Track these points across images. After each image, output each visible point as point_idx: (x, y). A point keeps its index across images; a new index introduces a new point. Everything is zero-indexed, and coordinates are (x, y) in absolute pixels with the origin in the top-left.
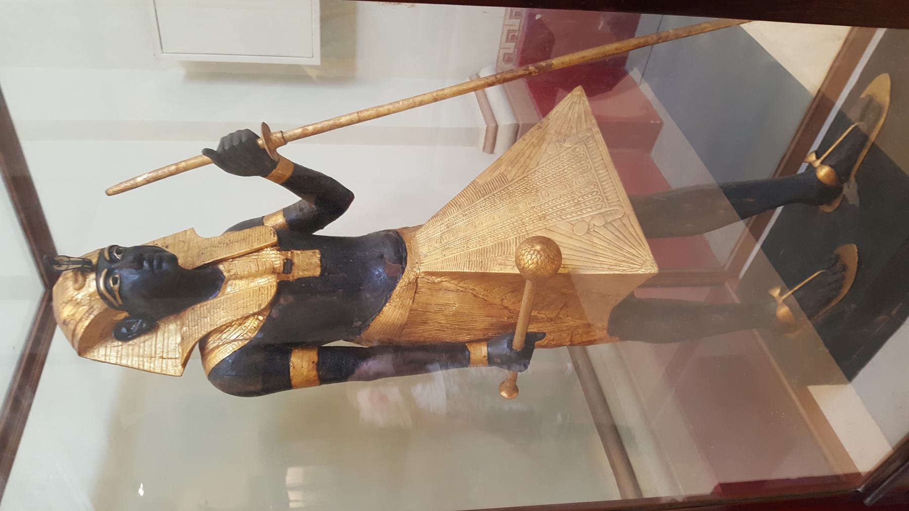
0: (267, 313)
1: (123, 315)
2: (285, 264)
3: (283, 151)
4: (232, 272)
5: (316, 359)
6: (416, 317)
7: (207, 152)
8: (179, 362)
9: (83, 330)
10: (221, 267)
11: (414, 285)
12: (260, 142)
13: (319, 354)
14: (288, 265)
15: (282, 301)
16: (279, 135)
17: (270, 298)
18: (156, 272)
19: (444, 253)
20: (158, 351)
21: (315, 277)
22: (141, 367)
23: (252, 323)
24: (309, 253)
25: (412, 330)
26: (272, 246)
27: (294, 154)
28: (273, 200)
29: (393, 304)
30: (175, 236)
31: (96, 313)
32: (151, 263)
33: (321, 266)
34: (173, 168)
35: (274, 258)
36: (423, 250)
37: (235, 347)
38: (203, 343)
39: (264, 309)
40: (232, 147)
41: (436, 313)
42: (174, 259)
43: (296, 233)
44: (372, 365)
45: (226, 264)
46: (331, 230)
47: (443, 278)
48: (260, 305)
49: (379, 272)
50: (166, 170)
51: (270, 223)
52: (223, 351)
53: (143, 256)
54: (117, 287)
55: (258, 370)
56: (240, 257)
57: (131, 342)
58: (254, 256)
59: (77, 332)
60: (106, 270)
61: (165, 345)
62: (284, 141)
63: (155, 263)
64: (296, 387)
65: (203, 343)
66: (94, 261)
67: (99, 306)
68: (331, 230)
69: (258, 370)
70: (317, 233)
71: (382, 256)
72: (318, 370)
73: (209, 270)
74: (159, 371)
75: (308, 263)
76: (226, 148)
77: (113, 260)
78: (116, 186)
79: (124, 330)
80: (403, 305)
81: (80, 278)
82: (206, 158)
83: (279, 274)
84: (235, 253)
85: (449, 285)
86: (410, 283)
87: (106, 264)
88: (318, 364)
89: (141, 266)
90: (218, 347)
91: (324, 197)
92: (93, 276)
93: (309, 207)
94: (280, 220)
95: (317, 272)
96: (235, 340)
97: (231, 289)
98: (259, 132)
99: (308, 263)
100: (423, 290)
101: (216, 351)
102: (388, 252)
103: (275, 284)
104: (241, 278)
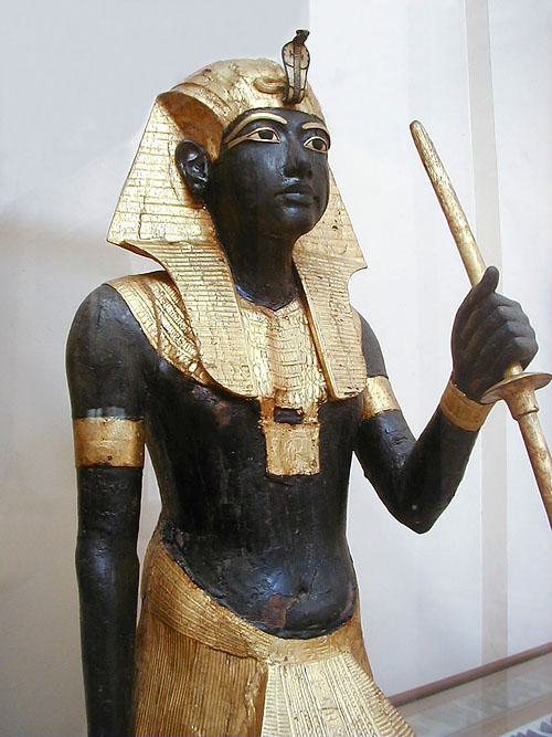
0: (201, 378)
1: (215, 155)
2: (294, 410)
3: (500, 412)
4: (283, 323)
5: (115, 463)
6: (182, 646)
7: (492, 277)
8: (132, 238)
9: (192, 95)
10: (295, 305)
11: (240, 652)
12: (515, 370)
13: (125, 467)
14: (291, 417)
15: (222, 405)
16: (531, 407)
17: (225, 384)
18: (280, 197)
19: (302, 717)
20: (155, 209)
21: (265, 465)
22: (130, 182)
23: (185, 354)
24: (314, 454)
25: (162, 641)
26: (329, 390)
27: (497, 429)
28: (414, 390)
29: (208, 610)
30: (354, 241)
31: (217, 111)
32: (292, 189)
33: (286, 477)
34: (461, 223)
35: (305, 394)
36: (315, 671)
37: (149, 328)
38: (164, 277)
39: (207, 374)
40: (503, 320)
41: (189, 693)
42: (304, 227)
43: (351, 429)
44: (102, 564)
45: (300, 313)
46: (361, 490)
47: (252, 711)
48: (214, 367)
49: (273, 584)
50: (456, 210)
51: (374, 386)
52: (137, 303)
53: (310, 184)
54: (256, 137)
55: (108, 365)
56: (311, 335)
57: (174, 168)
58: (311, 358)
59: (191, 88)
60: (285, 122)
61: (163, 219)
62: (519, 415)
63: (296, 196)
64: (75, 425)
65: (164, 277)
66: (302, 107)
67: (225, 114)
68: (361, 490)
69: (108, 365)
70: (355, 461)
71: (303, 589)
72: (96, 466)
73: (289, 286)
74: (121, 208)
75: (293, 452)
76: (502, 309)
77: (301, 133)
78: (426, 136)
79: (193, 156)
80: (204, 629)
81: (273, 86)
82: (480, 276)
83: (275, 400)
84: (319, 334)
85: (240, 721)
86: (247, 644)
87: (295, 124)
88: (107, 466)
89: (289, 174)
90: (152, 298)
91: (421, 480)
92: (276, 103)
93: (402, 452)
94: (379, 403)
95: (275, 469)
96: (159, 324)
97: (253, 322)
98: (535, 367)
99: (293, 452)
100: (232, 669)
101: (145, 297)
102: (311, 603)
103: (253, 394)
104: (270, 337)
